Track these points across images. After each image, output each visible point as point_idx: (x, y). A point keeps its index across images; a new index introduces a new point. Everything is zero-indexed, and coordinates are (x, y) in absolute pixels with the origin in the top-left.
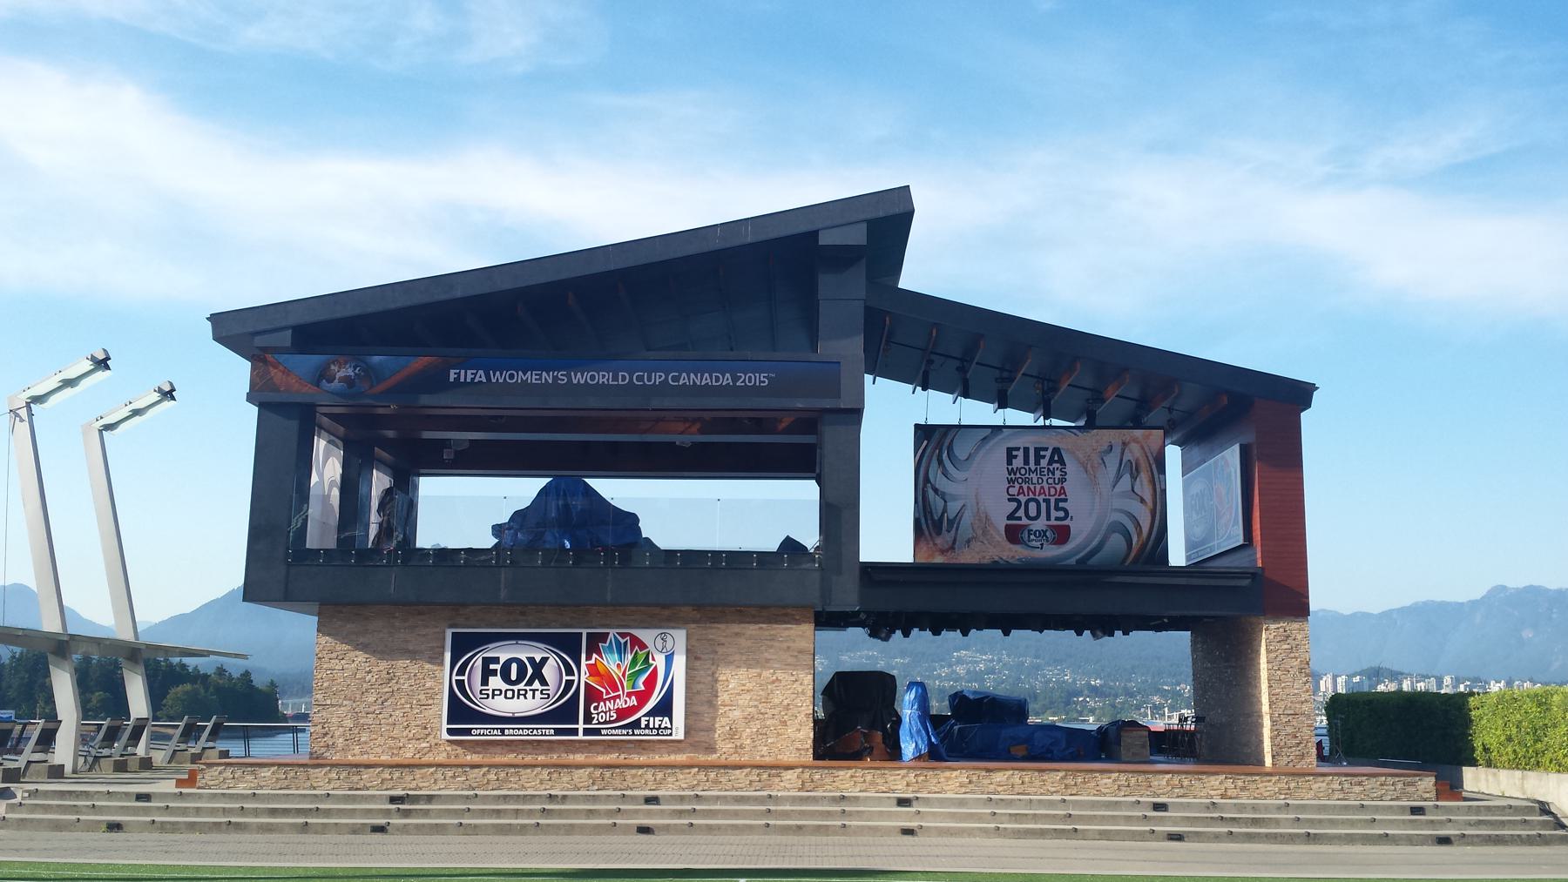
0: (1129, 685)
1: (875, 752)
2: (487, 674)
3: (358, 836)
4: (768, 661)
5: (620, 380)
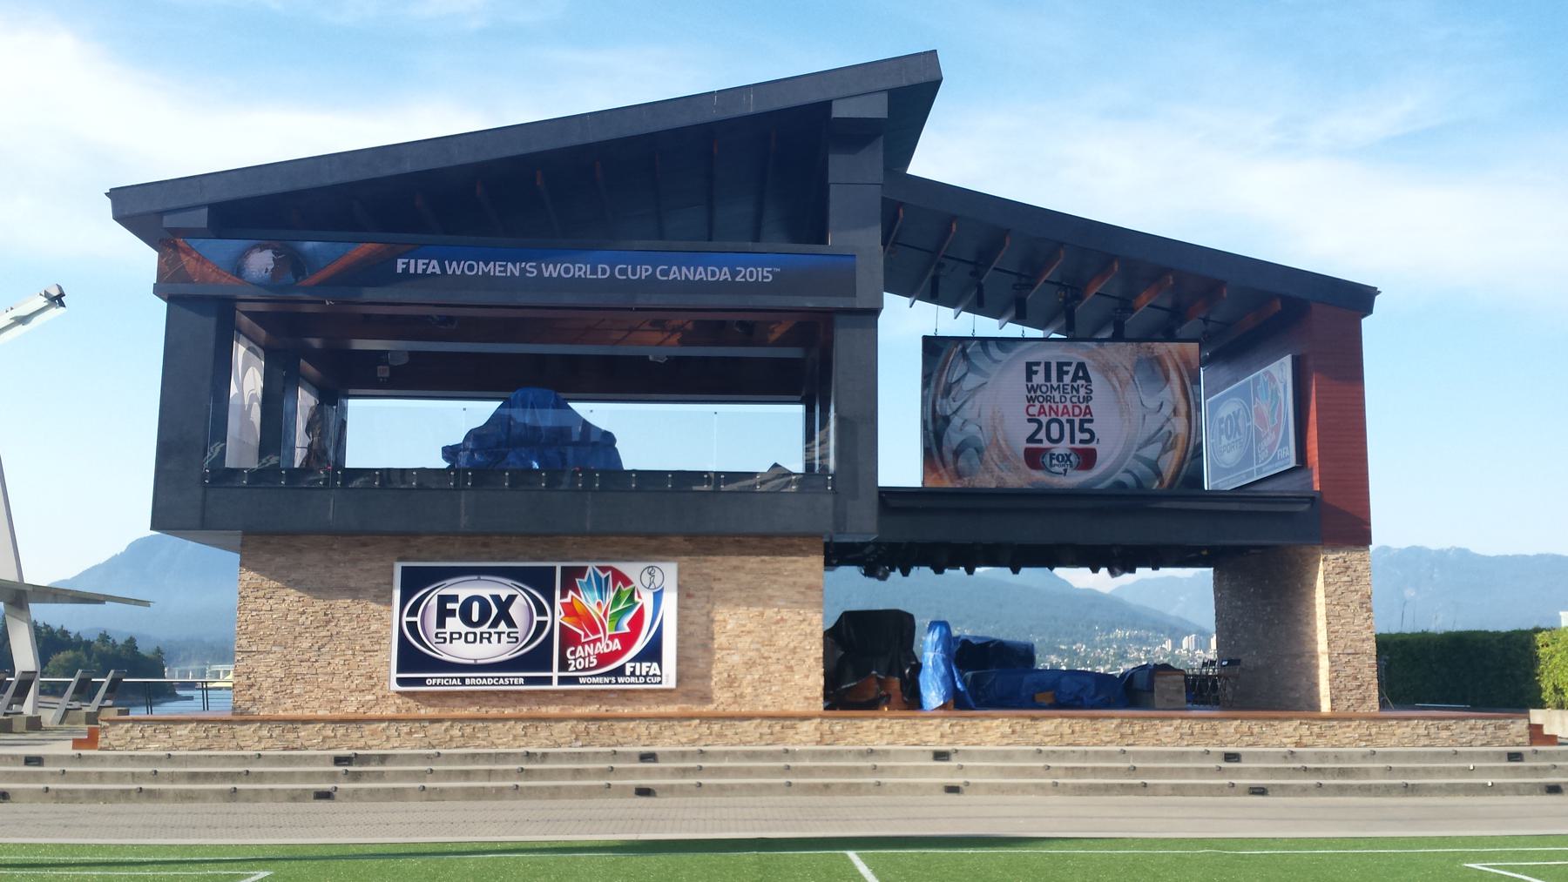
1: (893, 700)
2: (443, 614)
3: (298, 804)
4: (771, 598)
5: (600, 273)
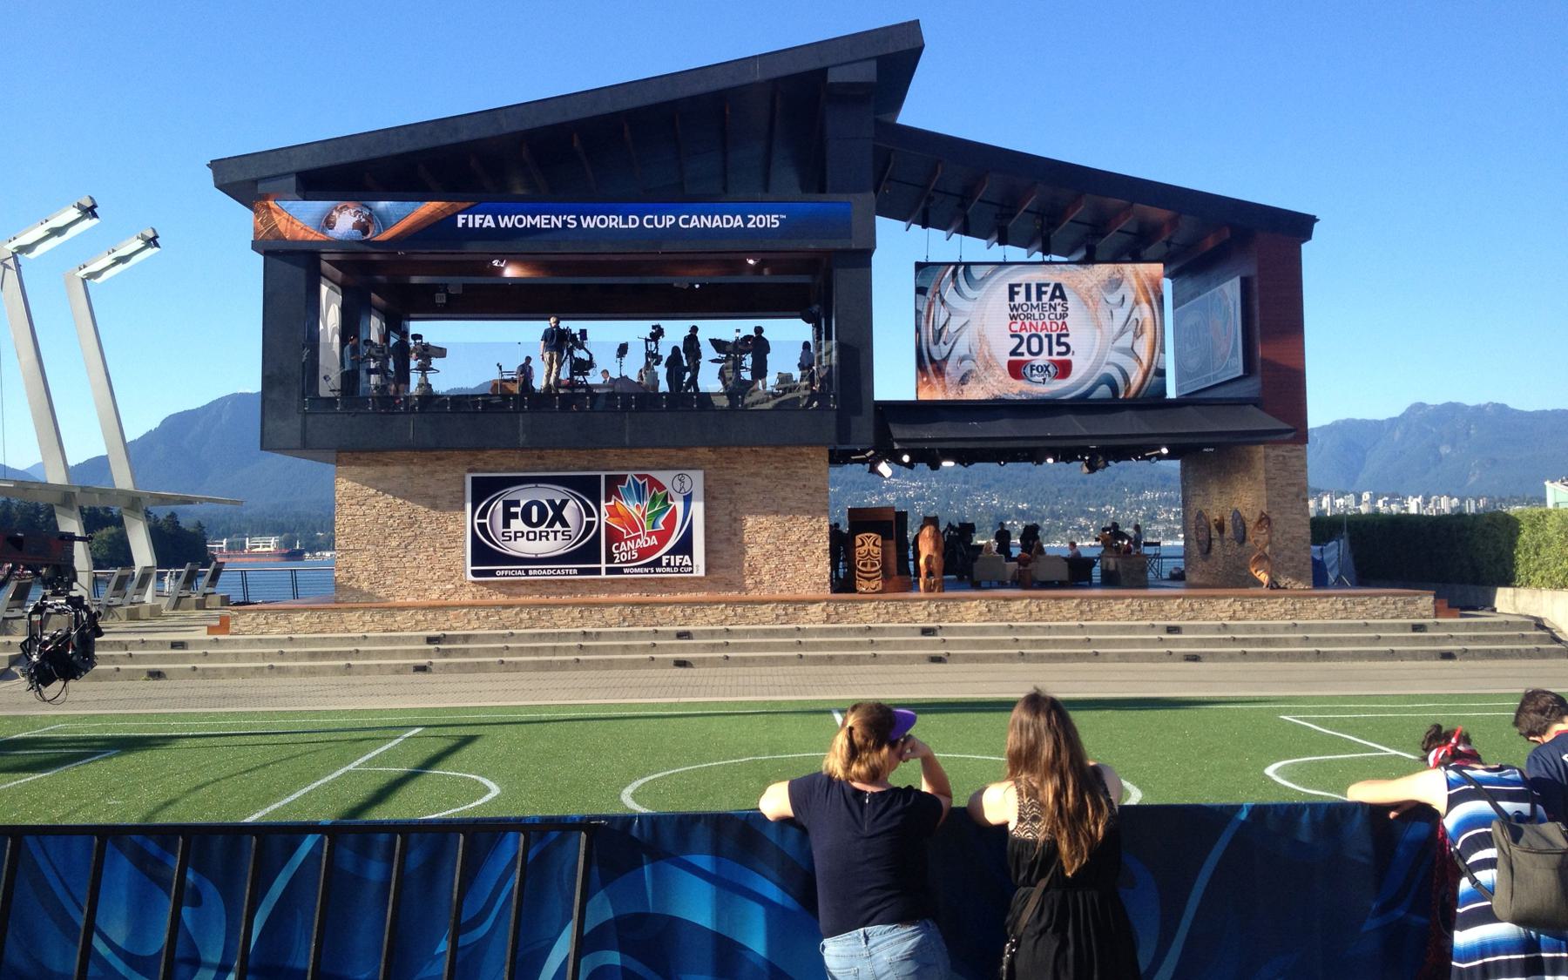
0: (1056, 508)
2: (508, 517)
